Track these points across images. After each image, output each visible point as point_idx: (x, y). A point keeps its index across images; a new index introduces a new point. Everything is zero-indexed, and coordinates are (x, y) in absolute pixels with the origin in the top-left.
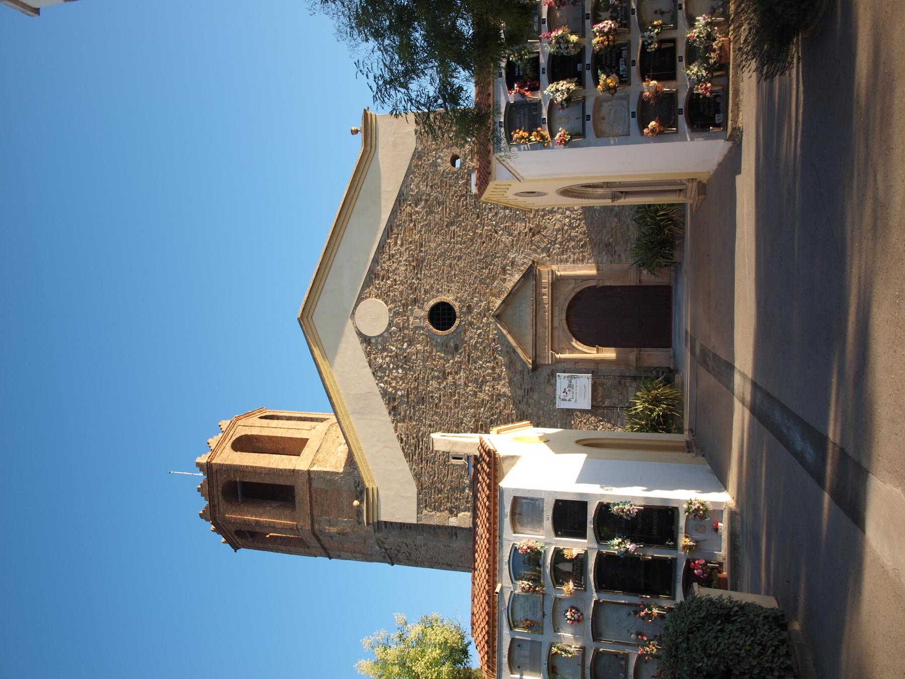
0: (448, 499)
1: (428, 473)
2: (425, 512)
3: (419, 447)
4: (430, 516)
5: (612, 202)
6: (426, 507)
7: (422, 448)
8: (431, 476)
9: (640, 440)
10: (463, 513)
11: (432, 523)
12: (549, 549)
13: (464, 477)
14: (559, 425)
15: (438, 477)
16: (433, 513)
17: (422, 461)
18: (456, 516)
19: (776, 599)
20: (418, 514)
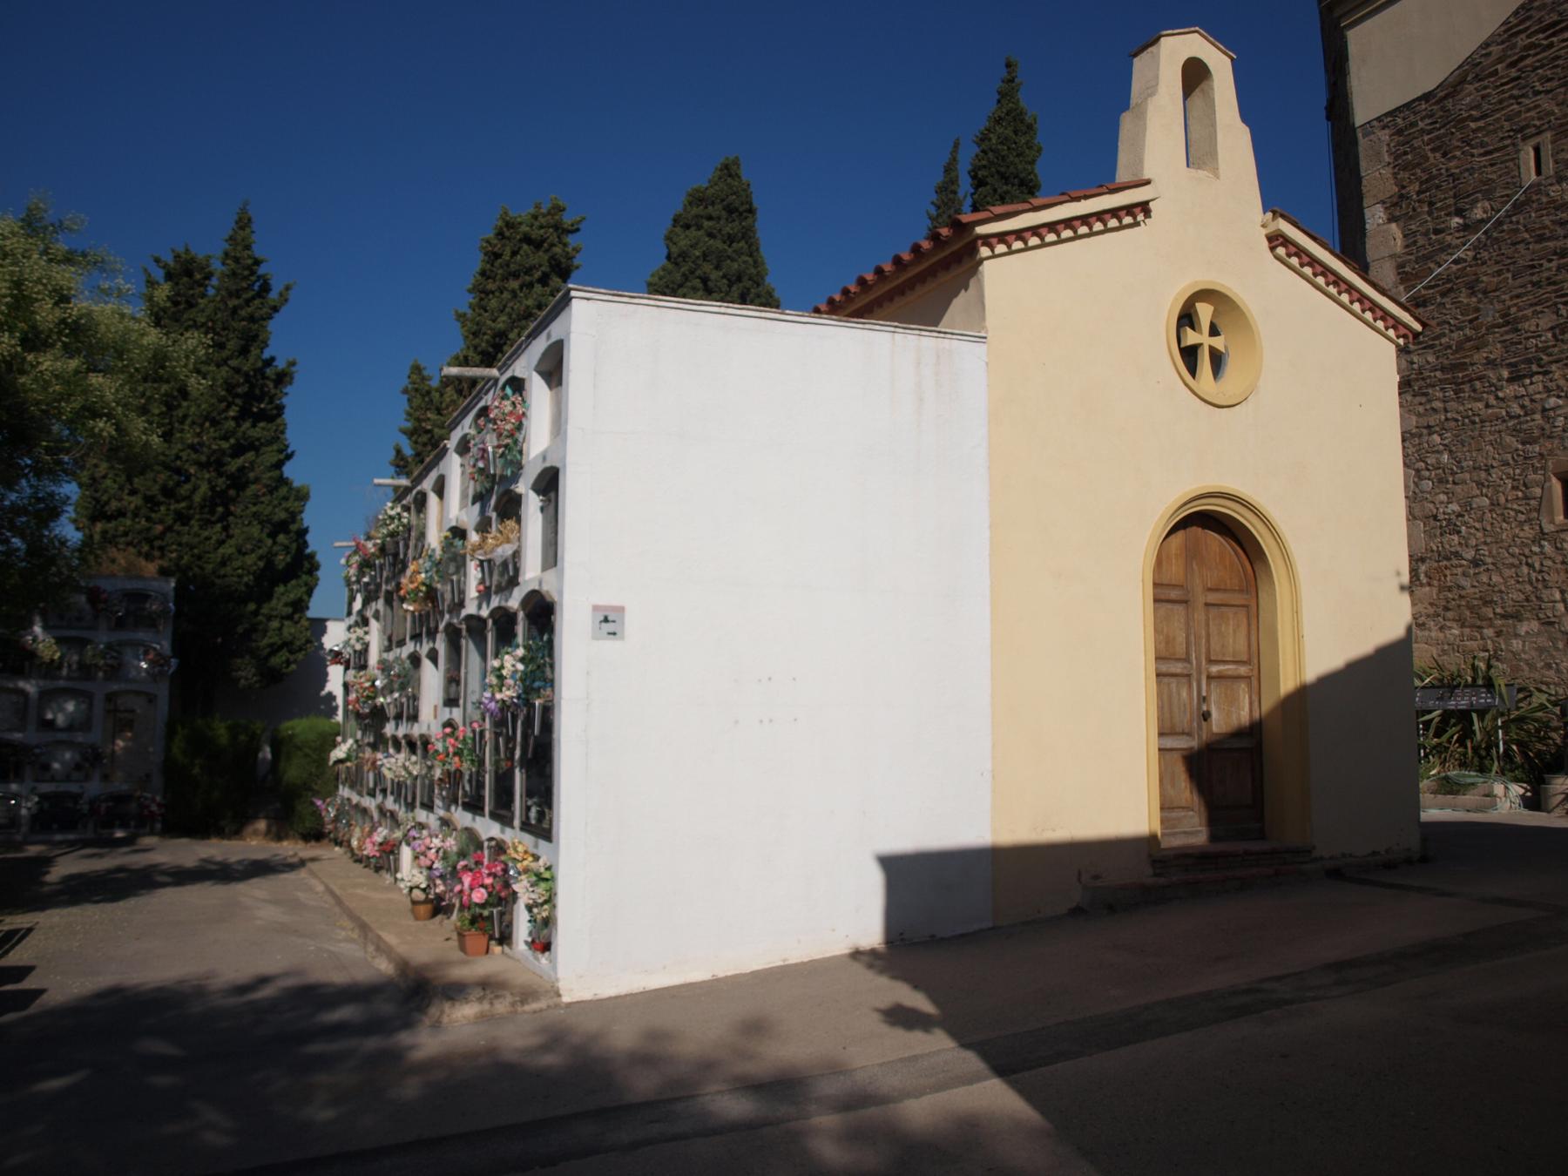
0: (1427, 181)
1: (1483, 97)
2: (1385, 135)
3: (1553, 35)
4: (1379, 153)
5: (473, 703)
6: (1400, 132)
7: (1551, 45)
8: (1477, 107)
9: (1298, 638)
10: (1399, 235)
11: (1363, 164)
12: (529, 636)
13: (1489, 200)
14: (158, 826)
15: (1479, 129)
16: (1387, 158)
17: (1512, 65)
18: (1391, 219)
19: (1135, 55)
20: (1379, 119)
